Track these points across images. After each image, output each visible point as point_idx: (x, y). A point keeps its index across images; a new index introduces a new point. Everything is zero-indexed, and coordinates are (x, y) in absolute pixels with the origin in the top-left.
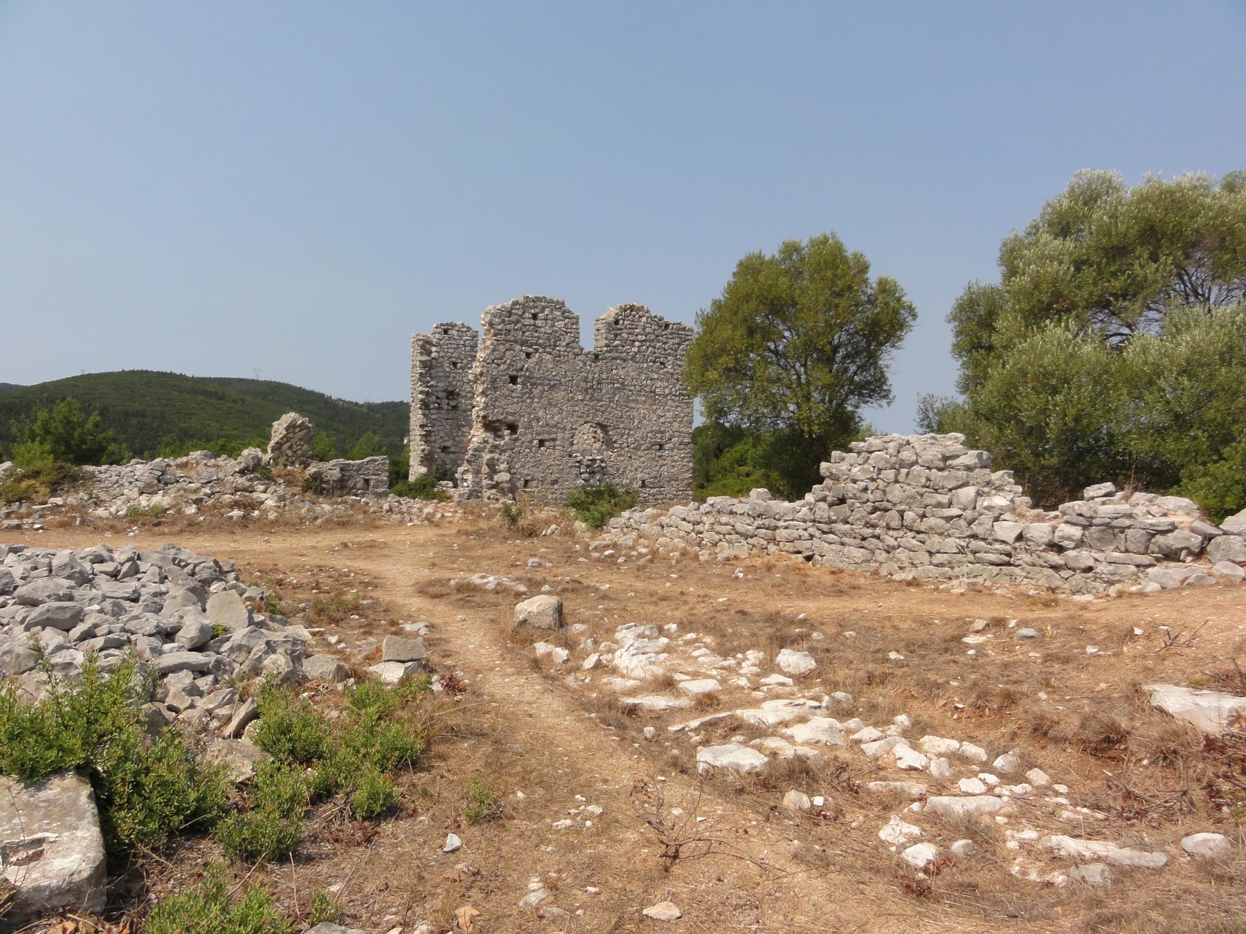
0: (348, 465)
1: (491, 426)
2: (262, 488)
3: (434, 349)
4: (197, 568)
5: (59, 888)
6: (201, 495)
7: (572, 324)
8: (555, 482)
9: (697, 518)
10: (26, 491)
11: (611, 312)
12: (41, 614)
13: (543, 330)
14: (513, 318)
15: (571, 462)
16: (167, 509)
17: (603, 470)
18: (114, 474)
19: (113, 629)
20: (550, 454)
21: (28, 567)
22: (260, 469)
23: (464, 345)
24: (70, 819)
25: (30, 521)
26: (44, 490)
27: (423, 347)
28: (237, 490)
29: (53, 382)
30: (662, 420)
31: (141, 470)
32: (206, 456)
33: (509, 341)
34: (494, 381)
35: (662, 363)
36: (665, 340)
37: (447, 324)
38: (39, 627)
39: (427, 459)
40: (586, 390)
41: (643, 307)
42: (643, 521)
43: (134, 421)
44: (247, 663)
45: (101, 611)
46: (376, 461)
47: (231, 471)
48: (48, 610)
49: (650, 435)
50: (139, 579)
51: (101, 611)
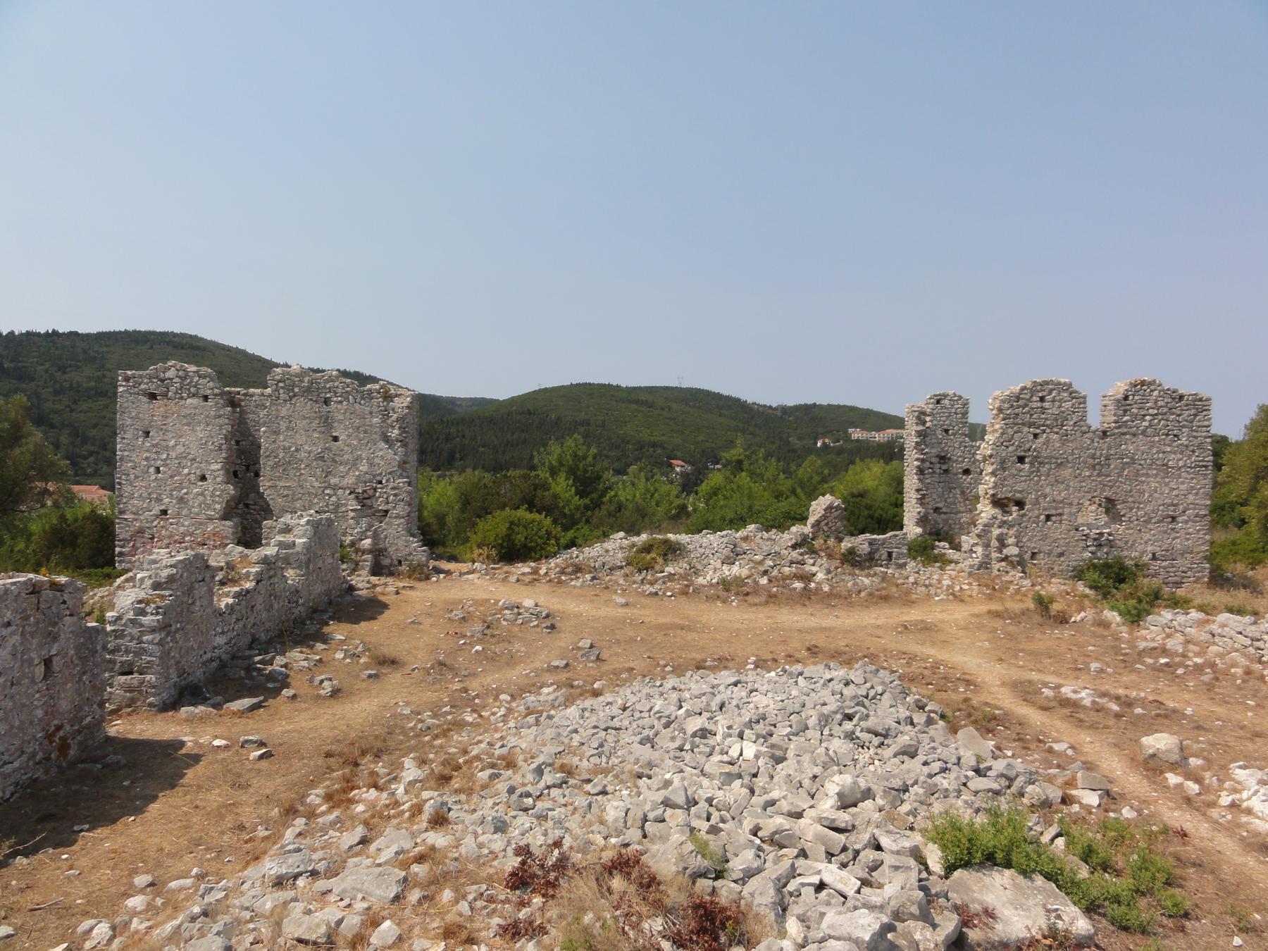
0: (875, 539)
1: (998, 503)
2: (811, 561)
3: (928, 419)
7: (1080, 404)
8: (1061, 555)
9: (1258, 635)
11: (1120, 387)
13: (1050, 411)
14: (1021, 402)
15: (1078, 536)
17: (1110, 544)
20: (1056, 528)
23: (956, 413)
26: (660, 560)
27: (918, 418)
28: (792, 562)
30: (1175, 493)
33: (1016, 424)
34: (1003, 462)
35: (1175, 436)
36: (1179, 412)
37: (940, 395)
39: (922, 521)
40: (1094, 467)
41: (1154, 381)
42: (1188, 624)
46: (896, 536)
49: (1161, 508)
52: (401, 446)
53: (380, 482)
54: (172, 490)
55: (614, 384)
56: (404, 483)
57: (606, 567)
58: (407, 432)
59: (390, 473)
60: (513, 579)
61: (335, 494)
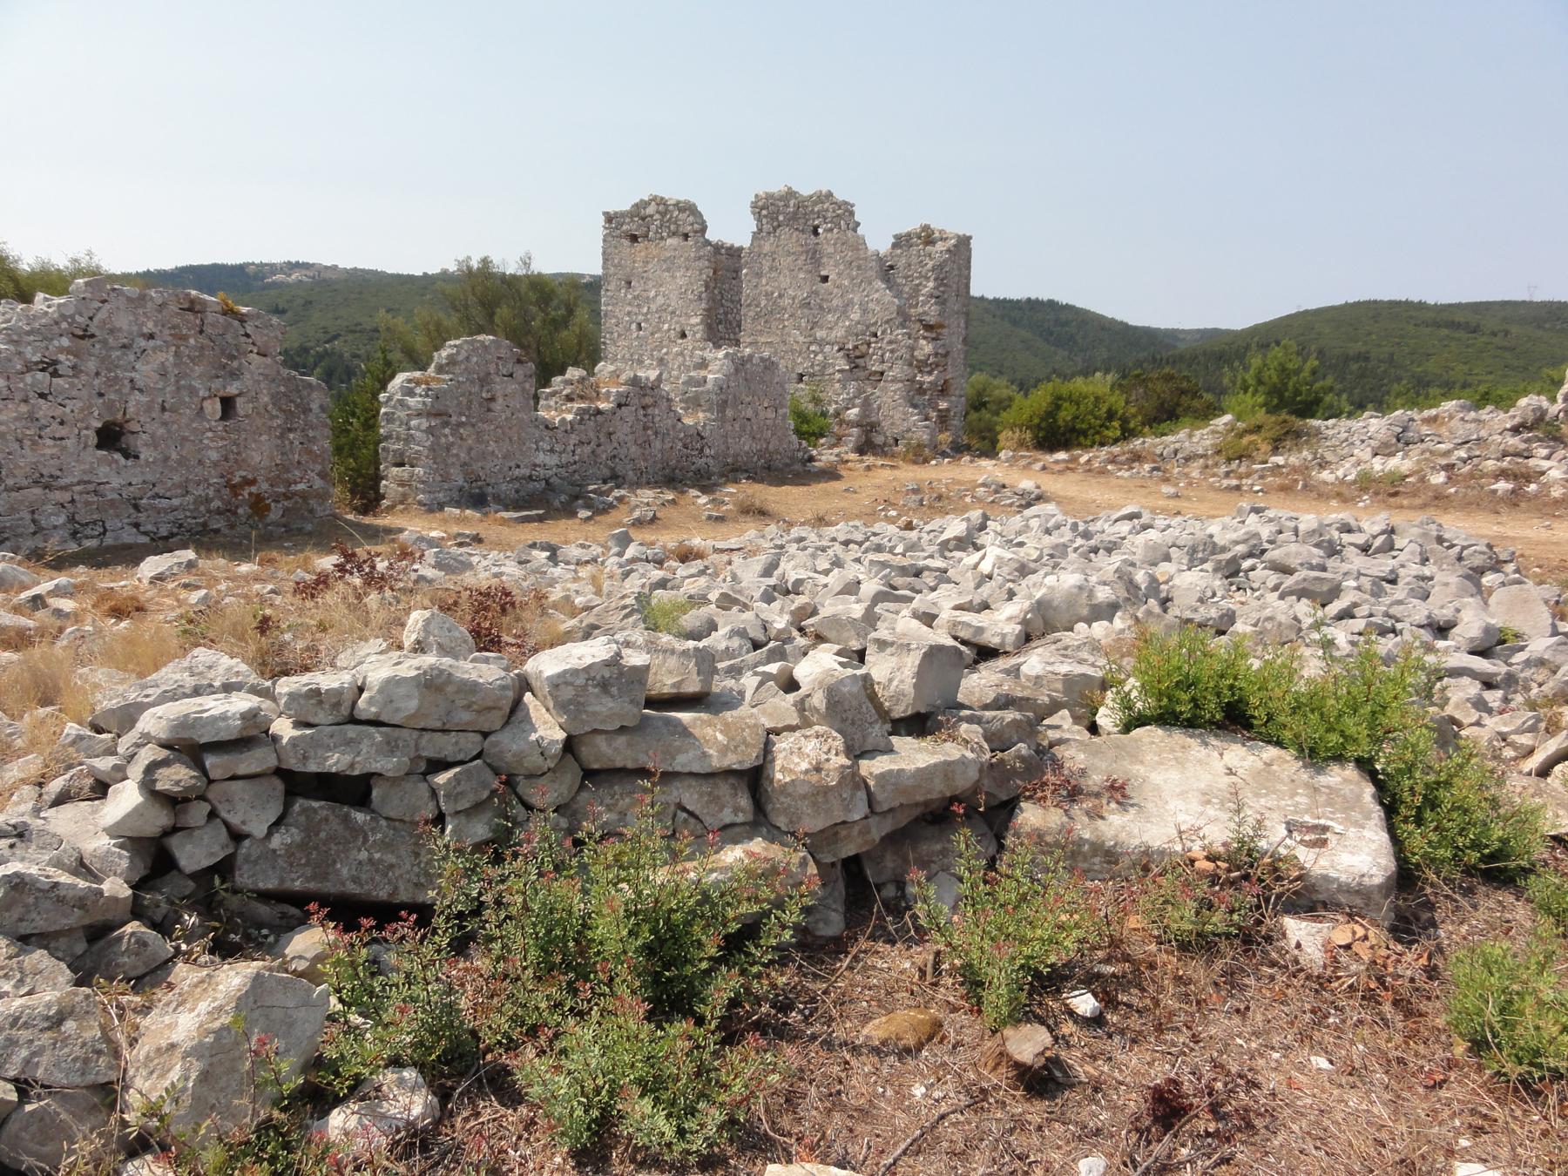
2: (1544, 452)
4: (1465, 552)
5: (1348, 885)
6: (1453, 459)
10: (1247, 448)
12: (1297, 583)
16: (1407, 476)
18: (1343, 430)
19: (1375, 612)
21: (1274, 529)
22: (1542, 425)
24: (1356, 815)
25: (1250, 482)
26: (1265, 447)
29: (1265, 323)
31: (1375, 425)
32: (1463, 407)
38: (1294, 597)
43: (1354, 367)
44: (1551, 684)
45: (1359, 588)
47: (1498, 427)
48: (1305, 580)
50: (1394, 557)
51: (1359, 588)
52: (936, 303)
53: (875, 335)
54: (652, 350)
55: (1416, 300)
56: (903, 334)
57: (1180, 455)
58: (945, 285)
59: (887, 322)
60: (1038, 466)
61: (822, 351)
